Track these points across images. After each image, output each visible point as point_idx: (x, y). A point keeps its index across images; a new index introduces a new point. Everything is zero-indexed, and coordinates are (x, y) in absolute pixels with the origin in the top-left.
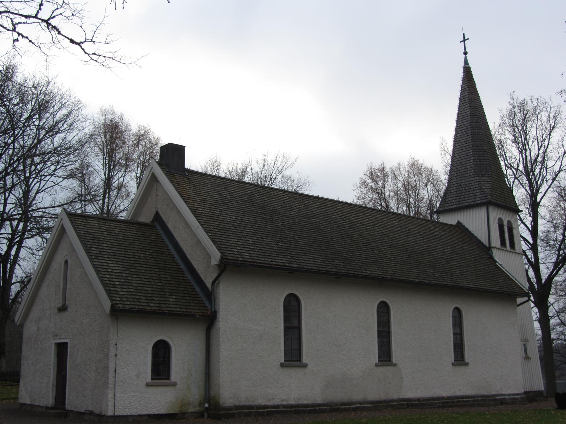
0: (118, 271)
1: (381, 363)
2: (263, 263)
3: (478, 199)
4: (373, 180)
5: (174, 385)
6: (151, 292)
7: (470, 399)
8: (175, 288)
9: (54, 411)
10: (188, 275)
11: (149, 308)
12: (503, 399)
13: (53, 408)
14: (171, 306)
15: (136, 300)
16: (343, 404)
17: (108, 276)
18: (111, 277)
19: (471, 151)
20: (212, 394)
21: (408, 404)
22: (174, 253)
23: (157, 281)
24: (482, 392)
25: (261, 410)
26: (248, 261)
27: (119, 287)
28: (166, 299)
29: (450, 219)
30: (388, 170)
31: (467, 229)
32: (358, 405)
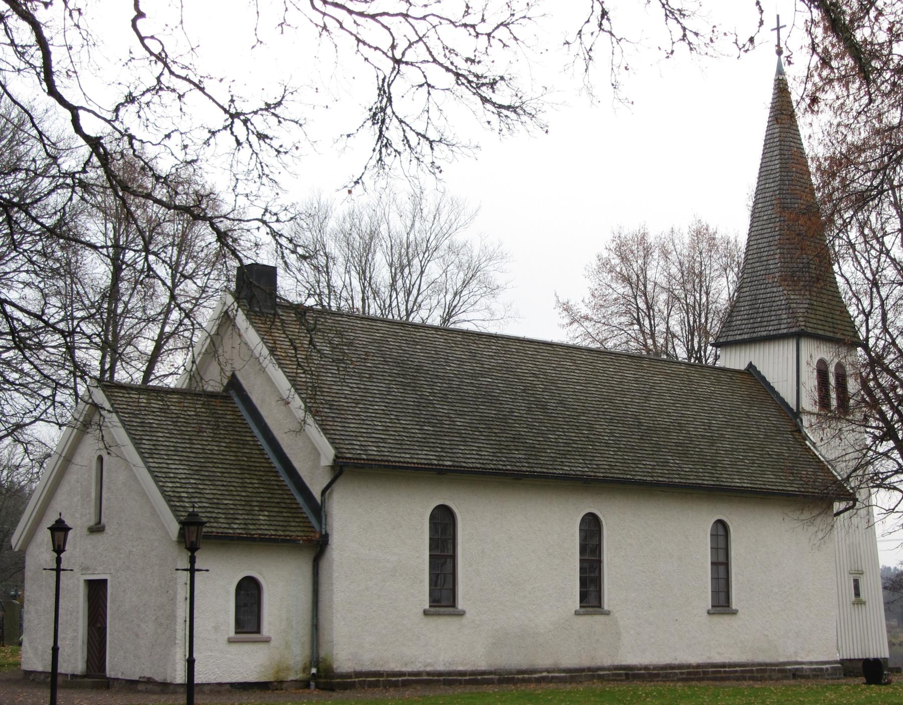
0: (183, 476)
1: (583, 610)
2: (399, 462)
3: (783, 326)
5: (267, 641)
6: (232, 507)
8: (266, 499)
9: (86, 680)
10: (284, 477)
11: (231, 531)
12: (797, 669)
14: (262, 527)
15: (212, 520)
17: (170, 485)
18: (174, 485)
20: (322, 654)
21: (627, 675)
22: (262, 441)
23: (239, 489)
24: (761, 658)
25: (394, 679)
27: (186, 500)
30: (651, 240)
31: (764, 378)
32: (545, 674)
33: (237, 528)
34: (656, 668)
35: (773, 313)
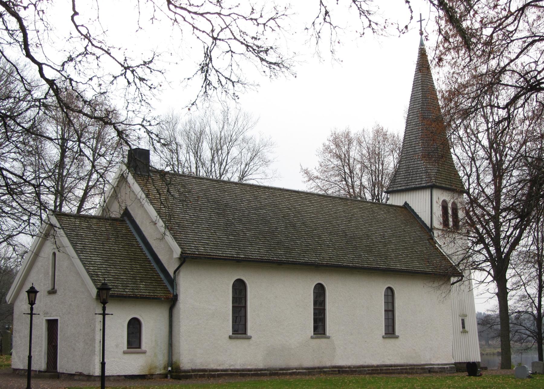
0: (99, 263)
1: (315, 336)
3: (423, 182)
4: (337, 146)
5: (144, 352)
7: (399, 368)
9: (47, 374)
10: (154, 264)
12: (431, 368)
13: (45, 372)
16: (281, 369)
17: (92, 268)
19: (420, 134)
20: (174, 359)
21: (339, 371)
22: (142, 244)
24: (411, 362)
26: (203, 255)
29: (397, 200)
30: (352, 135)
31: (413, 210)
32: (294, 371)
33: (128, 291)
34: (355, 367)
35: (418, 175)
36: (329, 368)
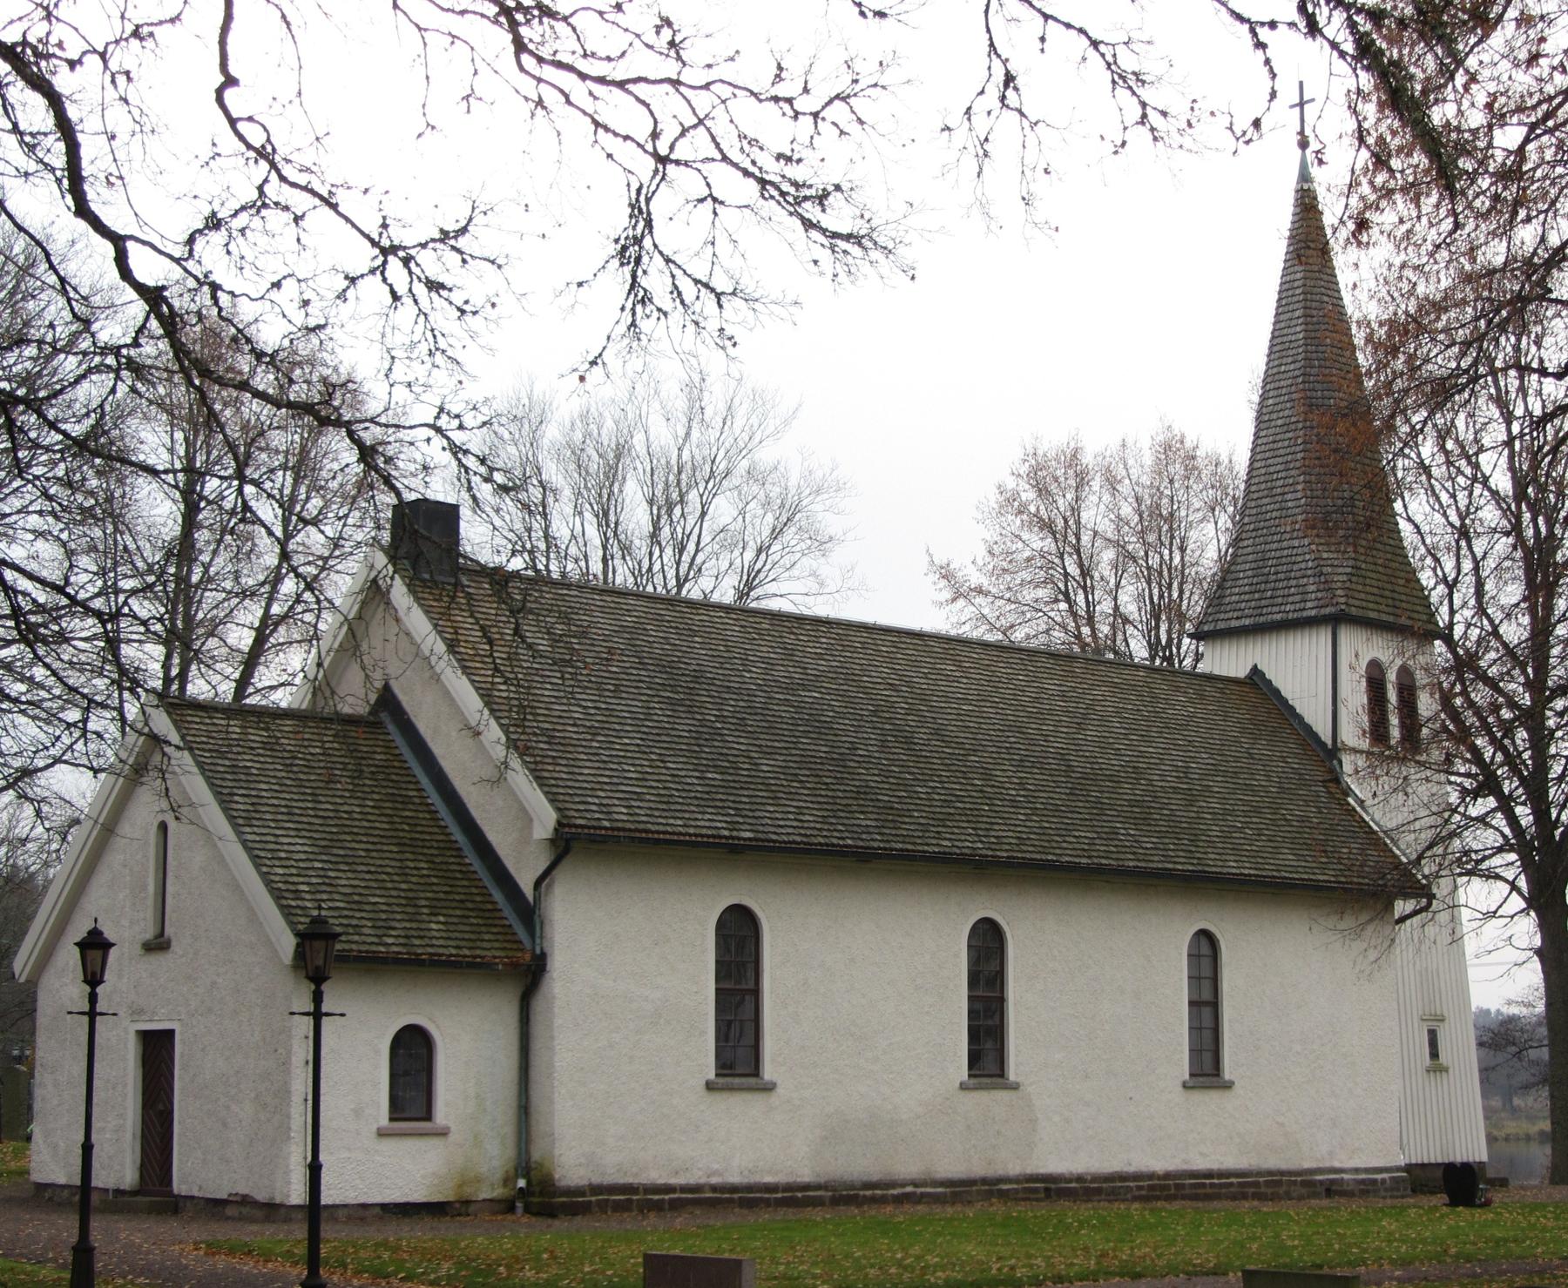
0: (303, 856)
1: (974, 1081)
2: (664, 833)
3: (1309, 605)
5: (443, 1133)
8: (442, 896)
10: (471, 858)
11: (382, 949)
12: (1333, 1181)
13: (134, 1193)
14: (435, 942)
17: (281, 871)
18: (287, 871)
20: (536, 1155)
21: (1047, 1190)
22: (434, 798)
24: (1273, 1162)
25: (656, 1197)
26: (624, 829)
27: (308, 896)
28: (423, 926)
29: (1229, 661)
30: (1087, 459)
31: (1277, 692)
32: (909, 1189)
33: (393, 944)
34: (1097, 1178)
35: (1294, 582)
36: (1016, 1180)
